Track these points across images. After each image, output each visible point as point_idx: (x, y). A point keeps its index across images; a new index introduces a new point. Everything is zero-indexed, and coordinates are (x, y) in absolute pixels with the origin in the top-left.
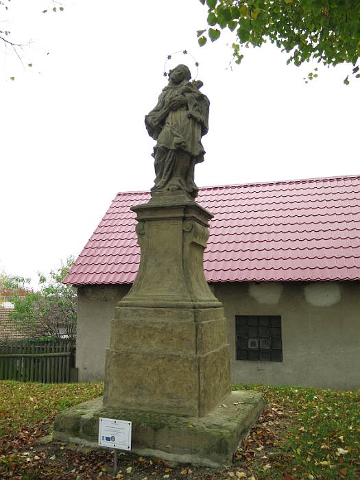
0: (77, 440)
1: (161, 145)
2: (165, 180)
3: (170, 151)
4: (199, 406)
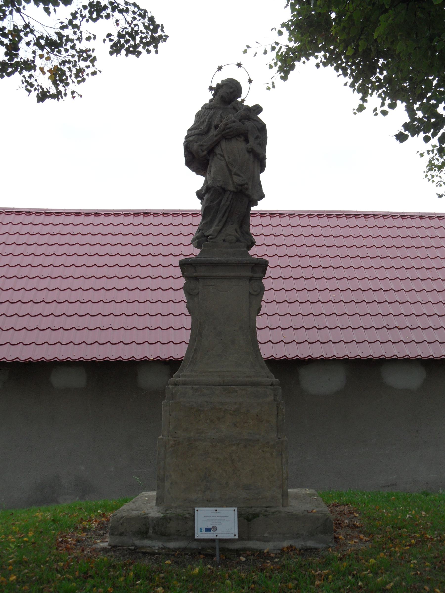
0: (147, 542)
1: (218, 184)
2: (219, 228)
3: (228, 193)
4: (282, 496)
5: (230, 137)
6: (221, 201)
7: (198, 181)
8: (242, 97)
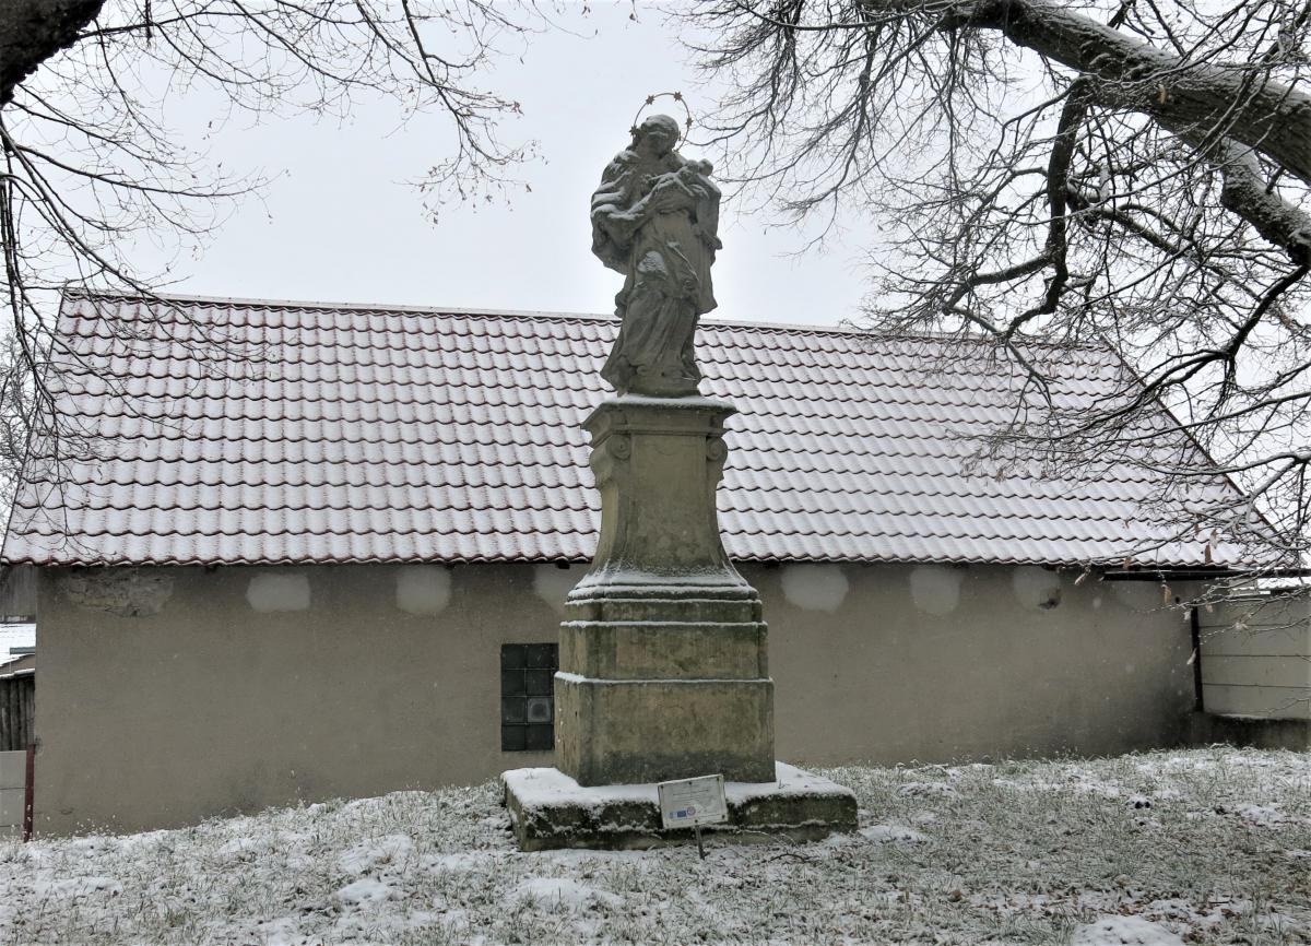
6: (657, 314)
7: (616, 281)
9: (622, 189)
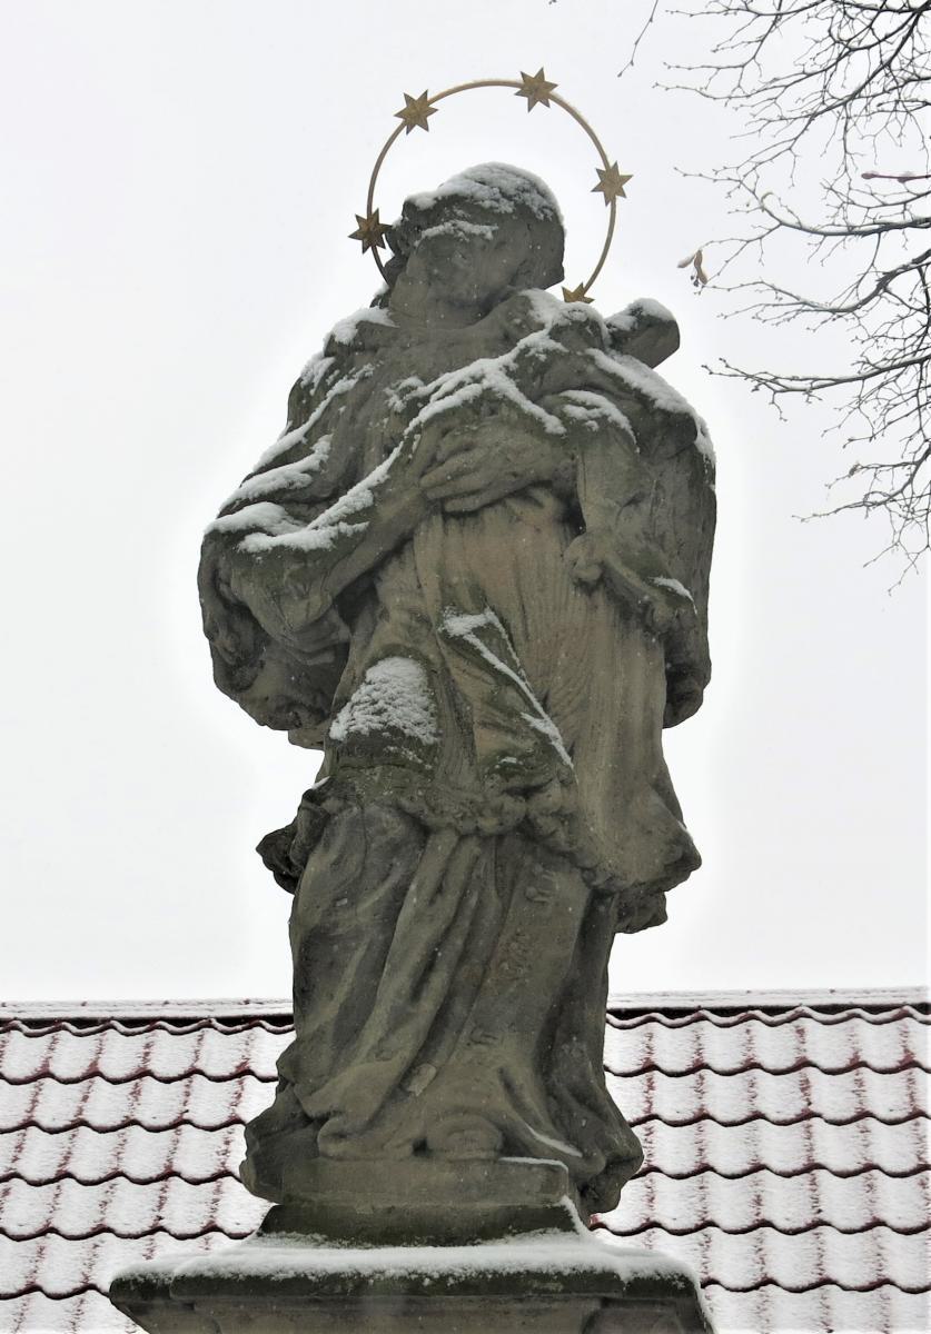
2: (395, 1065)
5: (471, 503)
6: (400, 893)
7: (279, 774)
8: (571, 281)
9: (322, 446)
